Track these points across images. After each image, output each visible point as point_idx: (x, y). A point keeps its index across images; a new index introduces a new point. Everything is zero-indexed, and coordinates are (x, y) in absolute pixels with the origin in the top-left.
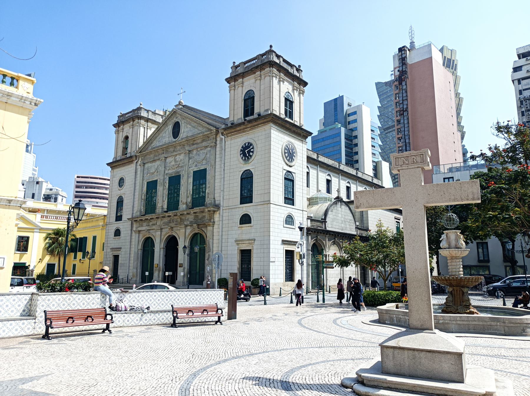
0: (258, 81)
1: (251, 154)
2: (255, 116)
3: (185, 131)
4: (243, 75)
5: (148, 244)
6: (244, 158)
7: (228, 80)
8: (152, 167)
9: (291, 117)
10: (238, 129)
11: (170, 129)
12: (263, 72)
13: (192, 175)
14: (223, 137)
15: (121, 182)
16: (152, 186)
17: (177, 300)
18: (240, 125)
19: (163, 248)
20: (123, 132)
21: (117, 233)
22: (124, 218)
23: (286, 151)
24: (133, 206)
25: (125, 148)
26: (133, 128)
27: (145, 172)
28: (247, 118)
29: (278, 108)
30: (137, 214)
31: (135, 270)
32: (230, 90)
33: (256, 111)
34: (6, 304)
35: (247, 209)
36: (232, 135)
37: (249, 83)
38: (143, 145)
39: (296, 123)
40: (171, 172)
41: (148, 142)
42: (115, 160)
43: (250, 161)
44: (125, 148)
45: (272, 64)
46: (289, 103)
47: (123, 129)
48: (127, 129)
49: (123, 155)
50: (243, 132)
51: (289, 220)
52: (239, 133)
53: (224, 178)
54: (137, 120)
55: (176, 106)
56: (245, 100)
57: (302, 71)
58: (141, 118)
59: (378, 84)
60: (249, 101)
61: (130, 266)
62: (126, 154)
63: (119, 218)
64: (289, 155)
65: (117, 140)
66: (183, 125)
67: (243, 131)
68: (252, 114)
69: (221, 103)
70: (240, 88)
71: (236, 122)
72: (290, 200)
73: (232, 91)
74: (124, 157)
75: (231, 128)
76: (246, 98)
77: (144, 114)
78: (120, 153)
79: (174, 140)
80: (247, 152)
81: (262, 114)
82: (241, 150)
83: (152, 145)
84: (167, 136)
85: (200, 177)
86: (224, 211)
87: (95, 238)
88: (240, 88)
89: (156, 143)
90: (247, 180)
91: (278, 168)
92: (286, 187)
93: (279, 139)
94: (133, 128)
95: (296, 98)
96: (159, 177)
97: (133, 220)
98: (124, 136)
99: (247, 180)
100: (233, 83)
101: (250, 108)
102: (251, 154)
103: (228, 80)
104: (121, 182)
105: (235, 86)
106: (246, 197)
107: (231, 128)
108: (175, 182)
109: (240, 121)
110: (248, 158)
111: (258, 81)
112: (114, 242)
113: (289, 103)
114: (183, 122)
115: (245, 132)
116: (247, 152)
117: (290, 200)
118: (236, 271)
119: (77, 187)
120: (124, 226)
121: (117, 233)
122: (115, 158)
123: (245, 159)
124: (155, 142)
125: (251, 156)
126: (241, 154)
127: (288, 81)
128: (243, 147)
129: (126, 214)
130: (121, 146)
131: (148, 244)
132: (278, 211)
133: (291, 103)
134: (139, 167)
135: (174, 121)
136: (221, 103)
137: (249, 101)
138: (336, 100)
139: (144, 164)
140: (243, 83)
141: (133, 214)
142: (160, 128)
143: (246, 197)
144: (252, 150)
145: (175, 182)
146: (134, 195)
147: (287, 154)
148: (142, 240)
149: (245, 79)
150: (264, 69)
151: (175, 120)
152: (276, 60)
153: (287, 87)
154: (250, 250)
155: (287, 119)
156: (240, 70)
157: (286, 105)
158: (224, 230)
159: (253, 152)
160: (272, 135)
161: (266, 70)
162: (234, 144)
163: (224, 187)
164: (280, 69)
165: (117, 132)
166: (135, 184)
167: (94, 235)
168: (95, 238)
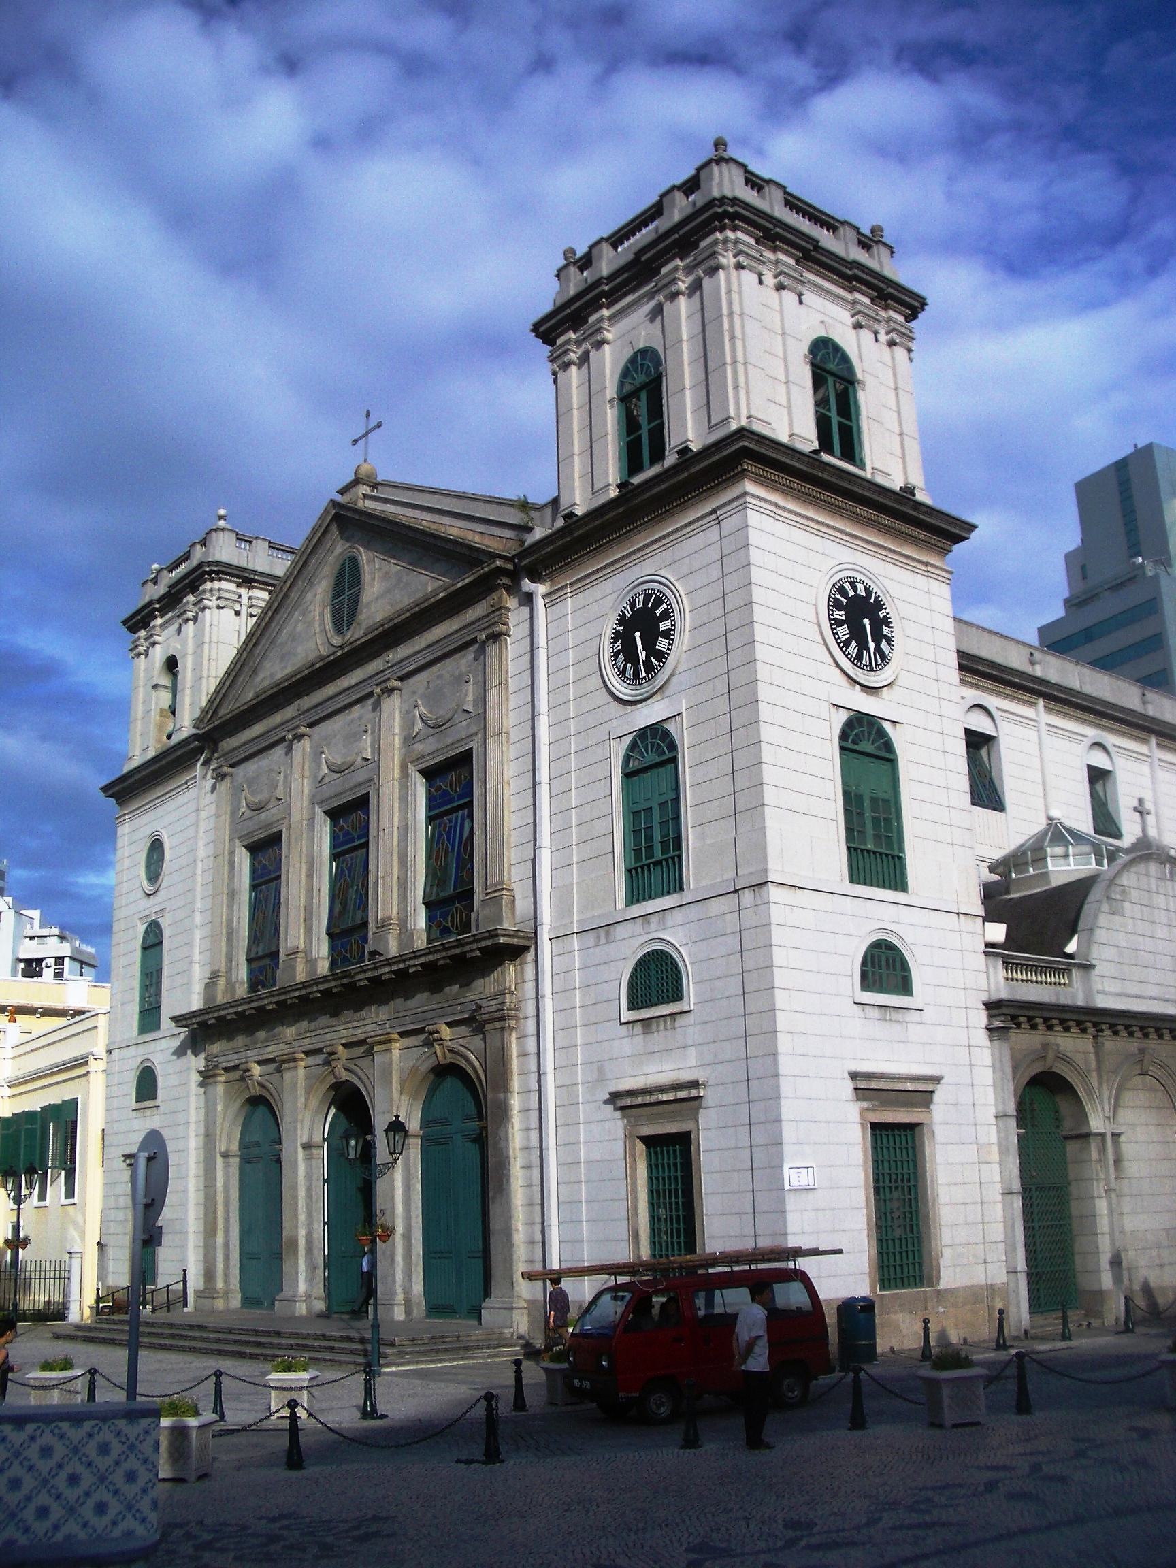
1: (662, 644)
2: (670, 459)
9: (850, 451)
13: (860, 890)
22: (166, 1024)
23: (840, 615)
28: (637, 480)
29: (785, 412)
33: (673, 441)
34: (97, 1496)
39: (880, 480)
45: (724, 214)
46: (832, 374)
51: (885, 968)
63: (149, 1017)
64: (860, 621)
68: (658, 454)
69: (534, 438)
72: (876, 850)
76: (628, 388)
77: (225, 550)
80: (642, 633)
82: (879, 605)
83: (261, 676)
85: (453, 784)
89: (275, 670)
90: (653, 755)
91: (801, 691)
92: (852, 801)
93: (788, 556)
95: (868, 355)
97: (203, 1030)
99: (653, 755)
102: (662, 644)
103: (547, 330)
106: (654, 859)
107: (575, 544)
110: (649, 668)
113: (832, 374)
116: (642, 633)
117: (876, 850)
118: (999, 1276)
121: (147, 1085)
124: (267, 664)
125: (661, 656)
132: (816, 921)
133: (885, 755)
138: (1121, 466)
142: (284, 593)
143: (654, 859)
144: (664, 626)
147: (843, 631)
152: (750, 196)
153: (826, 313)
155: (826, 458)
162: (558, 635)
164: (771, 234)
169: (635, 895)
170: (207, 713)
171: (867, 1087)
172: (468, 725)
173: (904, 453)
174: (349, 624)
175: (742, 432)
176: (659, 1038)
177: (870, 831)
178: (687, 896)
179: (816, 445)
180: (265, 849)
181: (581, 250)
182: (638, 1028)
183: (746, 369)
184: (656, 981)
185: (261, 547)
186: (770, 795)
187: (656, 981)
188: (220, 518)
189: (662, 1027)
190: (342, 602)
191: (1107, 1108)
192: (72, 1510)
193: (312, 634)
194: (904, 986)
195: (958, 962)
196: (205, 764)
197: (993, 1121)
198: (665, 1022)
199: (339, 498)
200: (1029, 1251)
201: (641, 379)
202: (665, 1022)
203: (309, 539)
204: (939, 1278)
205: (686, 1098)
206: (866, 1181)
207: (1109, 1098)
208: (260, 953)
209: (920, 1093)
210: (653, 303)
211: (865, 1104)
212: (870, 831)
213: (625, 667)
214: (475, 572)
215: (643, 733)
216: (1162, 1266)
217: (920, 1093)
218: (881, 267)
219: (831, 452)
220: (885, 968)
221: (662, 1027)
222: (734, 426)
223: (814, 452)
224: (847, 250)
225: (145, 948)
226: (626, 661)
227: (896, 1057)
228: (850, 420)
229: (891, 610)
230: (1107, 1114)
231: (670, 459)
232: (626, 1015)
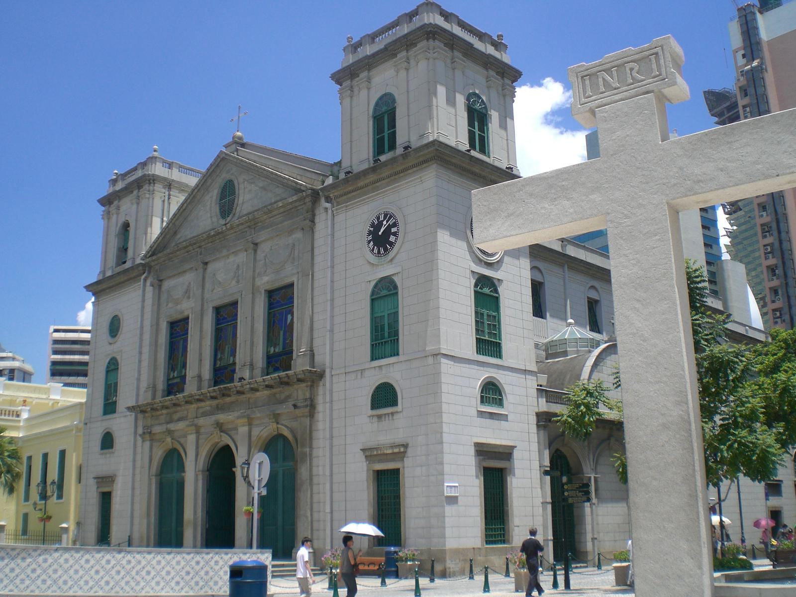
0: (403, 73)
2: (399, 151)
3: (248, 198)
4: (370, 63)
5: (172, 462)
6: (376, 251)
7: (339, 77)
8: (179, 283)
9: (483, 150)
10: (361, 183)
11: (214, 198)
12: (412, 52)
14: (328, 205)
15: (114, 327)
16: (178, 330)
17: (144, 573)
18: (364, 173)
19: (203, 471)
20: (118, 214)
21: (108, 442)
24: (138, 380)
25: (123, 250)
26: (138, 204)
27: (164, 297)
28: (383, 158)
30: (145, 398)
31: (145, 521)
32: (342, 99)
33: (401, 140)
35: (391, 371)
36: (350, 200)
37: (384, 79)
38: (161, 233)
39: (497, 164)
40: (217, 297)
41: (169, 233)
42: (101, 278)
43: (392, 254)
44: (123, 250)
47: (118, 208)
48: (127, 208)
49: (118, 265)
50: (373, 190)
51: (491, 392)
52: (365, 194)
53: (332, 300)
54: (146, 187)
55: (226, 146)
56: (374, 118)
57: (506, 46)
58: (152, 180)
59: (705, 92)
60: (385, 119)
61: (133, 503)
62: (125, 262)
63: (110, 407)
65: (107, 228)
66: (242, 186)
67: (373, 187)
68: (393, 146)
69: (321, 131)
70: (364, 92)
71: (357, 169)
72: (489, 344)
73: (347, 101)
74: (119, 269)
75: (346, 185)
77: (158, 170)
78: (112, 261)
79: (222, 222)
80: (382, 238)
81: (415, 144)
82: (370, 233)
83: (179, 236)
84: (206, 218)
85: (280, 301)
86: (335, 379)
87: (63, 453)
88: (364, 92)
89: (187, 233)
90: (385, 292)
94: (138, 204)
96: (187, 307)
97: (139, 410)
98: (120, 224)
99: (385, 292)
100: (347, 83)
101: (386, 134)
103: (339, 77)
104: (114, 327)
105: (351, 88)
106: (385, 339)
107: (346, 185)
108: (225, 316)
109: (365, 166)
111: (403, 73)
112: (102, 464)
113: (478, 118)
114: (241, 180)
115: (377, 189)
116: (382, 238)
117: (489, 344)
119: (55, 352)
120: (123, 425)
121: (108, 442)
122: (103, 272)
123: (379, 252)
126: (369, 242)
127: (480, 482)
128: (372, 225)
129: (126, 397)
130: (114, 244)
131: (172, 462)
132: (460, 384)
134: (149, 289)
135: (223, 181)
136: (321, 131)
137: (385, 119)
139: (206, 264)
140: (369, 80)
141: (138, 395)
143: (385, 339)
144: (393, 230)
145: (225, 316)
146: (140, 353)
148: (159, 454)
149: (373, 72)
150: (415, 45)
151: (225, 176)
153: (477, 79)
154: (398, 470)
155: (474, 153)
156: (369, 50)
157: (471, 124)
158: (335, 424)
159: (395, 234)
160: (441, 247)
161: (419, 45)
162: (343, 230)
163: (333, 326)
165: (107, 215)
166: (142, 327)
167: (62, 448)
168: (63, 453)
169: (374, 358)
170: (149, 252)
171: (483, 451)
172: (292, 269)
173: (508, 149)
174: (229, 214)
175: (436, 143)
176: (385, 423)
177: (486, 331)
178: (401, 358)
179: (467, 147)
180: (178, 330)
181: (356, 39)
182: (375, 419)
183: (437, 109)
184: (384, 397)
185: (175, 171)
186: (442, 312)
187: (384, 397)
188: (155, 151)
189: (387, 418)
190: (225, 203)
191: (592, 463)
192: (168, 563)
193: (206, 218)
194: (500, 403)
195: (523, 400)
196: (145, 280)
197: (541, 505)
198: (389, 416)
199: (224, 150)
200: (554, 531)
201: (384, 109)
202: (389, 416)
203: (208, 169)
204: (512, 541)
205: (401, 451)
206: (481, 502)
207: (593, 460)
208: (175, 376)
209: (506, 454)
210: (769, 449)
211: (481, 457)
212: (486, 331)
213: (374, 248)
214: (309, 198)
215: (382, 280)
216: (615, 541)
217: (506, 454)
218: (502, 57)
219: (475, 149)
220: (491, 392)
221: (387, 418)
222: (431, 139)
223: (468, 151)
224: (486, 49)
225: (108, 372)
226: (374, 245)
227: (494, 435)
228: (484, 133)
229: (366, 238)
230: (592, 468)
231: (399, 151)
232: (371, 412)
